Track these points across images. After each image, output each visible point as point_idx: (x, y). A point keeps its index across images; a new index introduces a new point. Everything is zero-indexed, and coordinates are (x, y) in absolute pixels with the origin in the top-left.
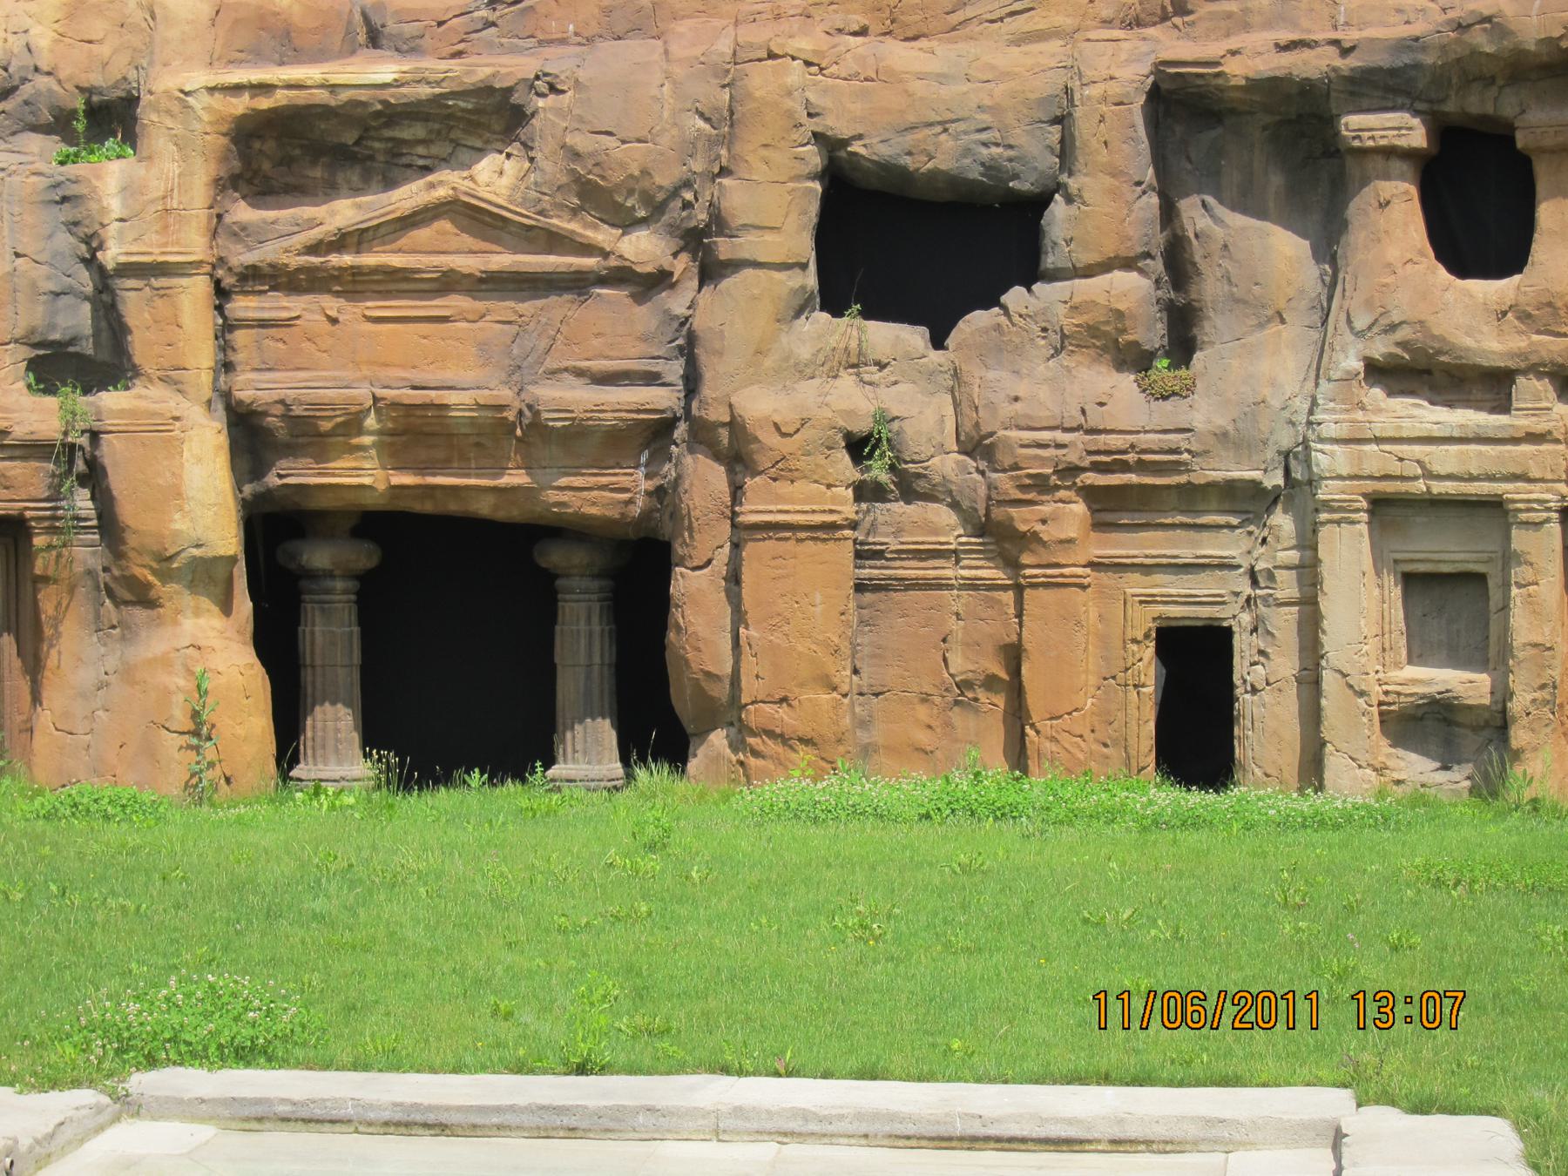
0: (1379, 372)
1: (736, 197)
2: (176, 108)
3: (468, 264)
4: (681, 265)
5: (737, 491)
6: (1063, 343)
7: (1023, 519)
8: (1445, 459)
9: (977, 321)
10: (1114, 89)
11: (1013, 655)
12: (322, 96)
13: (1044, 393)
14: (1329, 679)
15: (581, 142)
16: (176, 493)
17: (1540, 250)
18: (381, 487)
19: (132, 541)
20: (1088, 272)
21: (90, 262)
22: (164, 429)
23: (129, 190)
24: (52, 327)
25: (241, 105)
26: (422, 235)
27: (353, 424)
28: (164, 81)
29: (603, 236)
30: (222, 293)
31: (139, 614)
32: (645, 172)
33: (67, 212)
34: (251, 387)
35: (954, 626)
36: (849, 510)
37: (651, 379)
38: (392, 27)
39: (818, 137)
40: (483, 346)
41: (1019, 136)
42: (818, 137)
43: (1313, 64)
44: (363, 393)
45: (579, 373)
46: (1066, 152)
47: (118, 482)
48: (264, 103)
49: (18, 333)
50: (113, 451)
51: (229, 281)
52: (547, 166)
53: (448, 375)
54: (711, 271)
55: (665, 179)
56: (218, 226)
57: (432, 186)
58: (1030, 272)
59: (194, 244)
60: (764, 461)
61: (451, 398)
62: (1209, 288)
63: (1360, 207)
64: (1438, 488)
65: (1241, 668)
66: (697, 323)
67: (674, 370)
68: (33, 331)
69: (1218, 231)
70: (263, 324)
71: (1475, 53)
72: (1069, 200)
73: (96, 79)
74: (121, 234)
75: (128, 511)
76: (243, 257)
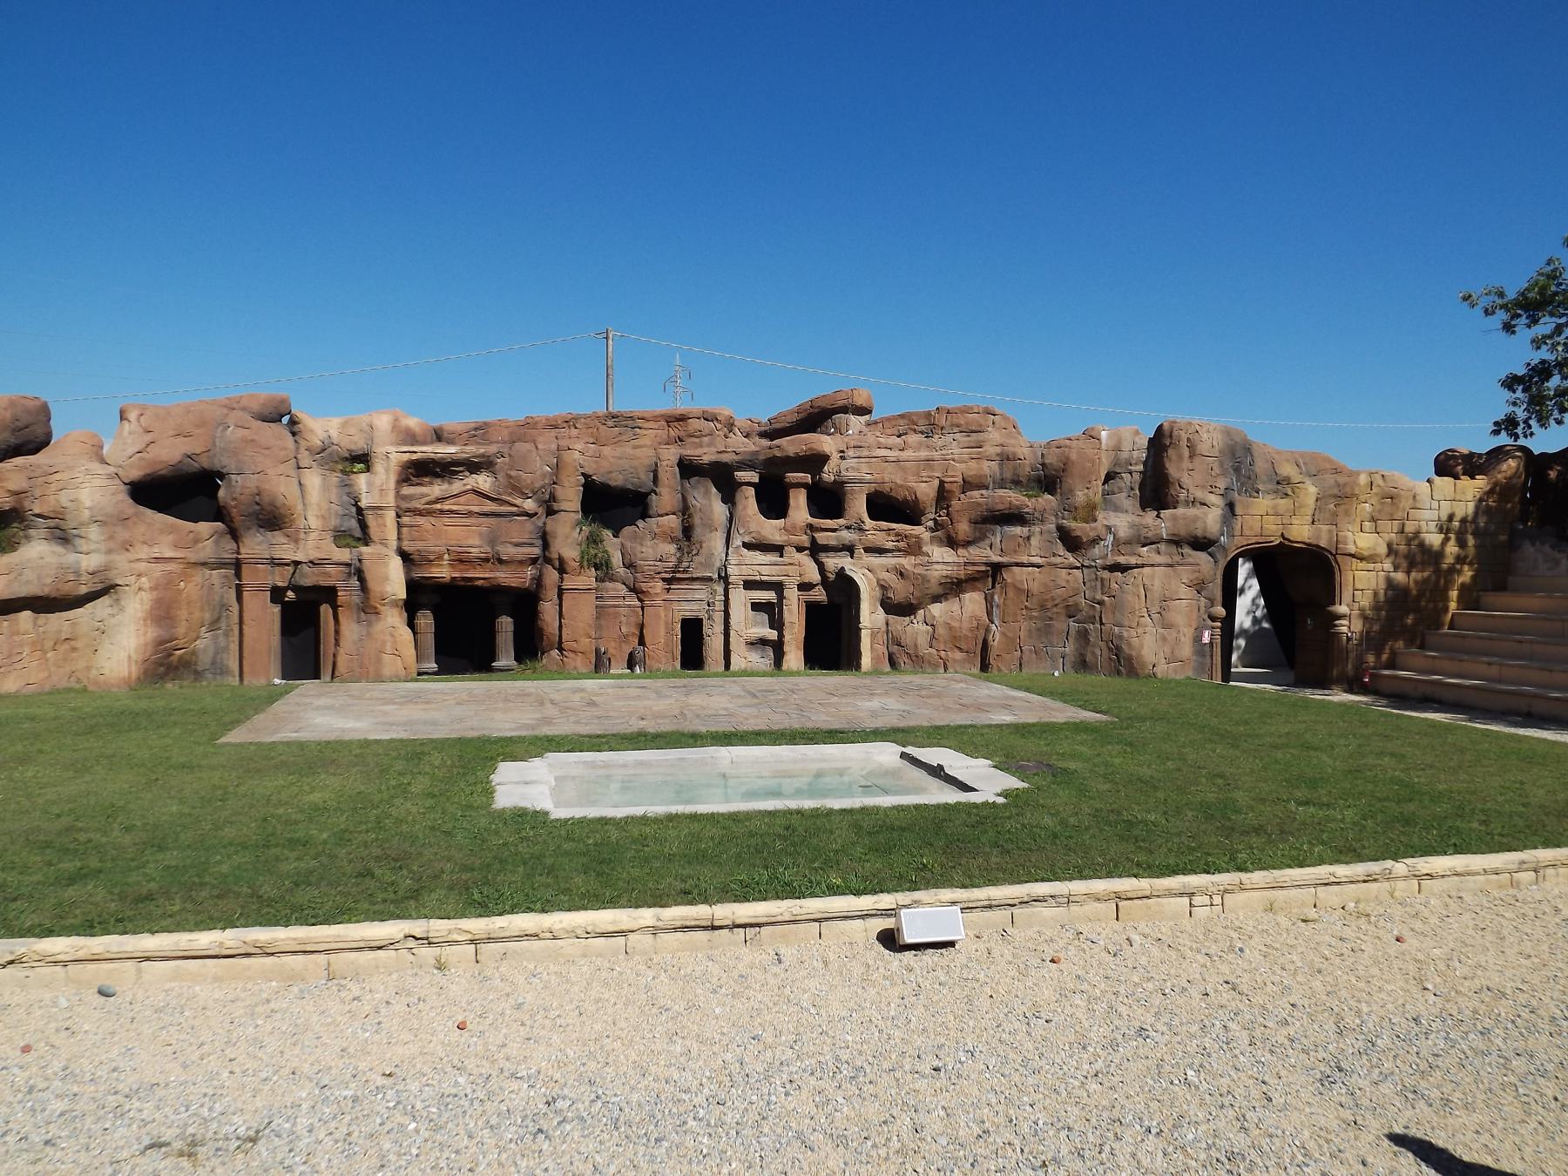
0: (746, 546)
1: (559, 492)
2: (384, 457)
3: (476, 509)
4: (541, 511)
5: (562, 579)
6: (655, 536)
7: (644, 586)
8: (765, 570)
9: (627, 530)
10: (670, 463)
11: (642, 627)
12: (432, 456)
13: (650, 551)
14: (732, 633)
15: (513, 473)
16: (386, 579)
17: (791, 512)
18: (449, 577)
19: (372, 594)
20: (662, 516)
21: (356, 505)
22: (382, 558)
23: (369, 484)
24: (342, 526)
25: (406, 457)
26: (462, 499)
27: (440, 557)
28: (380, 450)
29: (518, 501)
30: (398, 516)
31: (373, 617)
32: (532, 483)
33: (347, 489)
34: (407, 546)
35: (623, 619)
36: (594, 585)
37: (531, 545)
38: (445, 435)
39: (583, 474)
40: (480, 535)
41: (643, 476)
42: (583, 474)
43: (726, 458)
44: (444, 549)
45: (510, 543)
46: (656, 480)
47: (368, 576)
48: (414, 457)
49: (331, 528)
50: (366, 565)
51: (401, 513)
52: (501, 480)
53: (471, 542)
54: (551, 512)
55: (537, 485)
56: (398, 495)
57: (465, 485)
58: (645, 515)
59: (390, 500)
60: (569, 570)
61: (472, 550)
62: (697, 521)
63: (739, 497)
64: (764, 578)
65: (705, 629)
66: (548, 528)
67: (539, 542)
68: (336, 527)
69: (698, 505)
70: (412, 526)
71: (775, 456)
72: (656, 494)
73: (353, 447)
74: (367, 497)
75: (372, 584)
76: (405, 505)
